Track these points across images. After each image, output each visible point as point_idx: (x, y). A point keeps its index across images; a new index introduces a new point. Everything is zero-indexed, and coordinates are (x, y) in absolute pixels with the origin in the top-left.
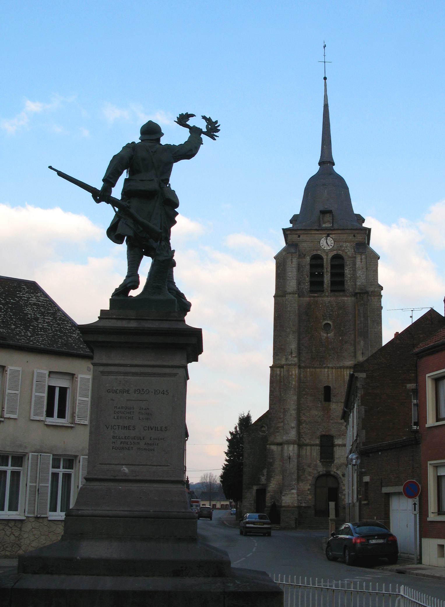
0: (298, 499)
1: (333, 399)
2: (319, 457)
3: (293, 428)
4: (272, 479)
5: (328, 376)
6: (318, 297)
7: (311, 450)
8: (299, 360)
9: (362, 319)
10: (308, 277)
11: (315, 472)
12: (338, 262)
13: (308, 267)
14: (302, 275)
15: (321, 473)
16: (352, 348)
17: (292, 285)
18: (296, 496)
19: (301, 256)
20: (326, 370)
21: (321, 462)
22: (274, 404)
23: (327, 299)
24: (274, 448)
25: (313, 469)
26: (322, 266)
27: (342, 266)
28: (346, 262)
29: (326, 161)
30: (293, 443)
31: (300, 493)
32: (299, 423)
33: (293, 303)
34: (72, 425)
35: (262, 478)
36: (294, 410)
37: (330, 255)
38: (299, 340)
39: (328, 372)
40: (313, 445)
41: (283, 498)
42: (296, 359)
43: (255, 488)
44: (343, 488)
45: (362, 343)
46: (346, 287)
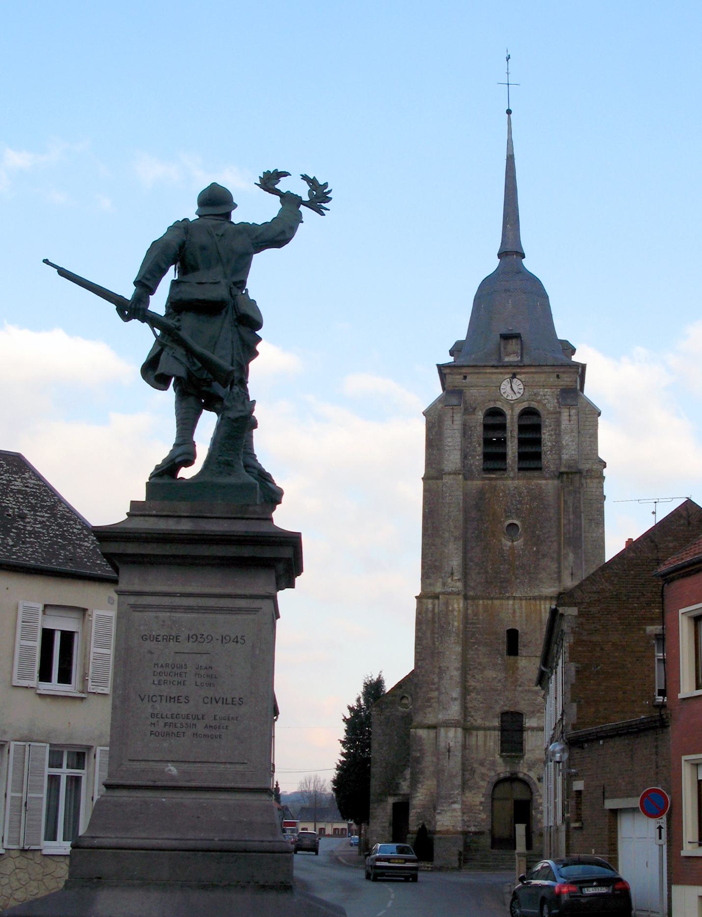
0: (463, 820)
1: (522, 650)
2: (498, 749)
3: (456, 699)
4: (420, 786)
5: (514, 612)
6: (497, 479)
7: (485, 736)
8: (466, 585)
9: (571, 517)
10: (479, 445)
11: (493, 774)
12: (531, 423)
13: (480, 429)
14: (470, 443)
15: (502, 776)
16: (554, 566)
17: (453, 459)
18: (459, 813)
19: (469, 410)
20: (511, 602)
21: (501, 756)
22: (424, 659)
23: (513, 482)
24: (422, 733)
25: (489, 769)
26: (503, 427)
27: (537, 428)
28: (545, 421)
29: (511, 252)
30: (456, 725)
31: (467, 809)
32: (466, 691)
33: (455, 489)
34: (83, 695)
35: (403, 783)
36: (457, 669)
37: (518, 410)
38: (465, 552)
39: (513, 605)
40: (489, 729)
41: (438, 817)
42: (459, 585)
43: (391, 800)
44: (539, 801)
45: (571, 557)
46: (544, 461)
